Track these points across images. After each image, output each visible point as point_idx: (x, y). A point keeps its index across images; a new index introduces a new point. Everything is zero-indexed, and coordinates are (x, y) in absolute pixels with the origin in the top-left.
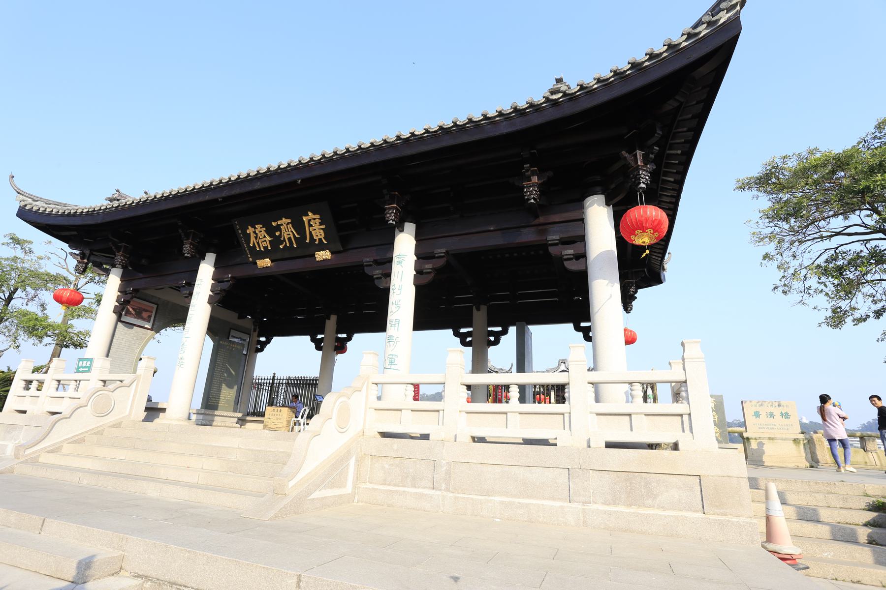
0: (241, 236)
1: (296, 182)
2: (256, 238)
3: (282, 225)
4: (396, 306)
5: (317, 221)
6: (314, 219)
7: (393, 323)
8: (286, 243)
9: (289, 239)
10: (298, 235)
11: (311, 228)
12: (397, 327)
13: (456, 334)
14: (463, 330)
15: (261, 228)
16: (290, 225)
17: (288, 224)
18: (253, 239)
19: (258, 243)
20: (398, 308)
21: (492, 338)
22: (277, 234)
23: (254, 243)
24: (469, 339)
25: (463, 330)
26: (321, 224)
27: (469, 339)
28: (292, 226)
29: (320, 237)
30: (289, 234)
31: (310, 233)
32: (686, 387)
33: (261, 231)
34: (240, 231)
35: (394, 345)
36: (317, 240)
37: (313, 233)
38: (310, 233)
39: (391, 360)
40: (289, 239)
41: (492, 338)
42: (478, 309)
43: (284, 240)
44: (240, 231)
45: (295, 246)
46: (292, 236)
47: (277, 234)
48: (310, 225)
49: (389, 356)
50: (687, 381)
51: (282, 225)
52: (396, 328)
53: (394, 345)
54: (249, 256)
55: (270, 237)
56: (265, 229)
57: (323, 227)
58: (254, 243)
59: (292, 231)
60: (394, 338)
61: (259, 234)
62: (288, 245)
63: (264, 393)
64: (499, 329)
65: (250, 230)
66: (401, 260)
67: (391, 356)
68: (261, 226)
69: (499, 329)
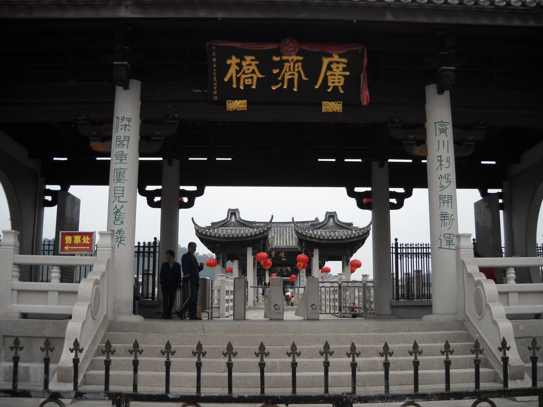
0: (215, 65)
1: (352, 21)
2: (238, 72)
3: (287, 61)
4: (447, 180)
5: (342, 66)
6: (338, 63)
7: (446, 199)
8: (283, 85)
9: (291, 81)
10: (306, 76)
11: (329, 73)
12: (451, 203)
13: (351, 194)
14: (149, 188)
15: (252, 60)
16: (300, 64)
17: (297, 61)
18: (232, 71)
19: (238, 79)
20: (449, 182)
21: (185, 200)
22: (275, 71)
23: (231, 78)
24: (157, 199)
25: (357, 190)
26: (344, 70)
27: (157, 199)
28: (302, 66)
29: (337, 84)
30: (294, 75)
31: (326, 78)
32: (511, 295)
33: (250, 65)
34: (214, 60)
35: (450, 224)
36: (331, 88)
37: (330, 78)
38: (326, 78)
39: (448, 239)
40: (291, 81)
41: (185, 200)
42: (126, 87)
43: (282, 81)
44: (214, 60)
45: (295, 90)
46: (296, 77)
47: (275, 71)
48: (329, 68)
49: (445, 235)
50: (221, 290)
51: (287, 61)
52: (450, 204)
53: (450, 224)
54: (215, 93)
55: (261, 73)
56: (257, 62)
57: (348, 73)
58: (231, 78)
59: (299, 72)
60: (450, 216)
61: (245, 68)
62: (285, 87)
63: (146, 259)
64: (194, 188)
65: (233, 61)
66: (444, 128)
67: (449, 235)
68: (254, 58)
69: (194, 188)
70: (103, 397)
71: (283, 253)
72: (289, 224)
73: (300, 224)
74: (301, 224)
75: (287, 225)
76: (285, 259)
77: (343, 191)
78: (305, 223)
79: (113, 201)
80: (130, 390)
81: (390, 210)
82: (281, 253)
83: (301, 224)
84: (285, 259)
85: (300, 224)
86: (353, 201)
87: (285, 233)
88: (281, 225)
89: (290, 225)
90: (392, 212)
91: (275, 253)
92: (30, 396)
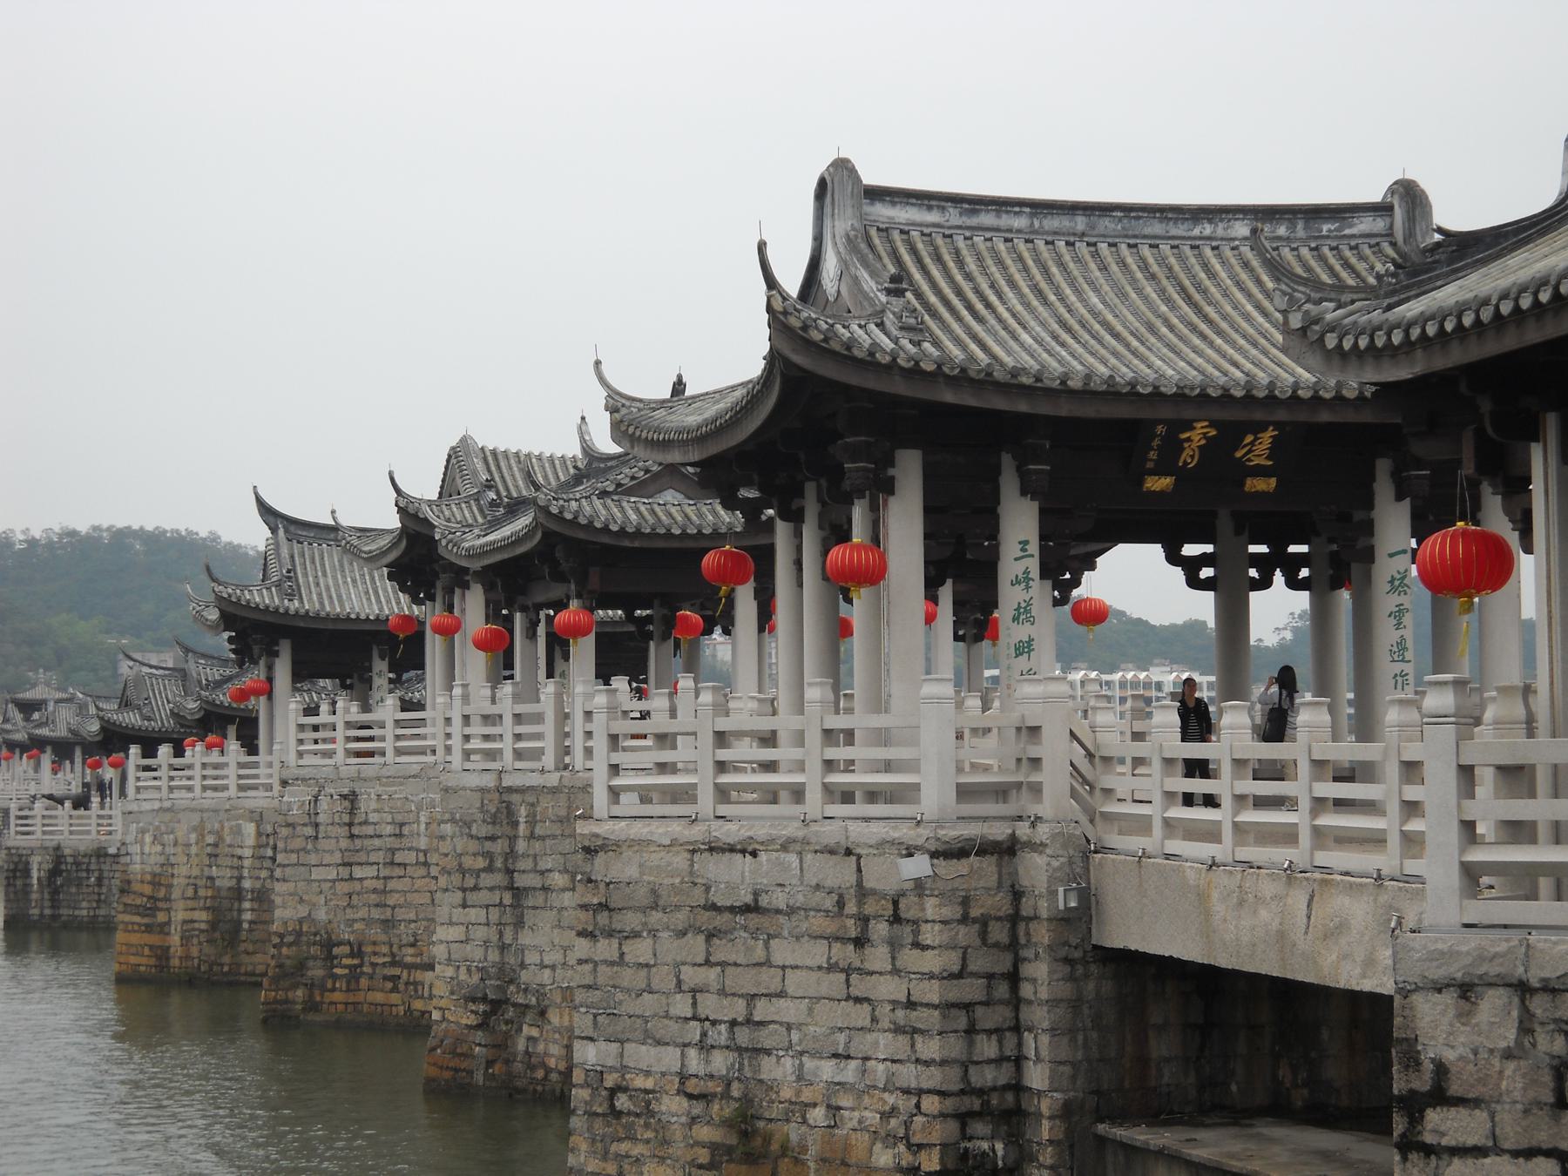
13: (1174, 558)
70: (1473, 616)
71: (1267, 437)
72: (1210, 221)
73: (1293, 228)
74: (1300, 225)
75: (1196, 232)
76: (1273, 482)
77: (1155, 551)
78: (1327, 220)
79: (604, 367)
80: (1006, 987)
81: (1251, 593)
82: (1249, 438)
83: (1300, 225)
84: (1273, 482)
85: (1293, 228)
86: (1178, 573)
87: (1238, 269)
88: (1157, 228)
89: (1220, 232)
90: (1253, 595)
91: (1213, 433)
92: (761, 629)
